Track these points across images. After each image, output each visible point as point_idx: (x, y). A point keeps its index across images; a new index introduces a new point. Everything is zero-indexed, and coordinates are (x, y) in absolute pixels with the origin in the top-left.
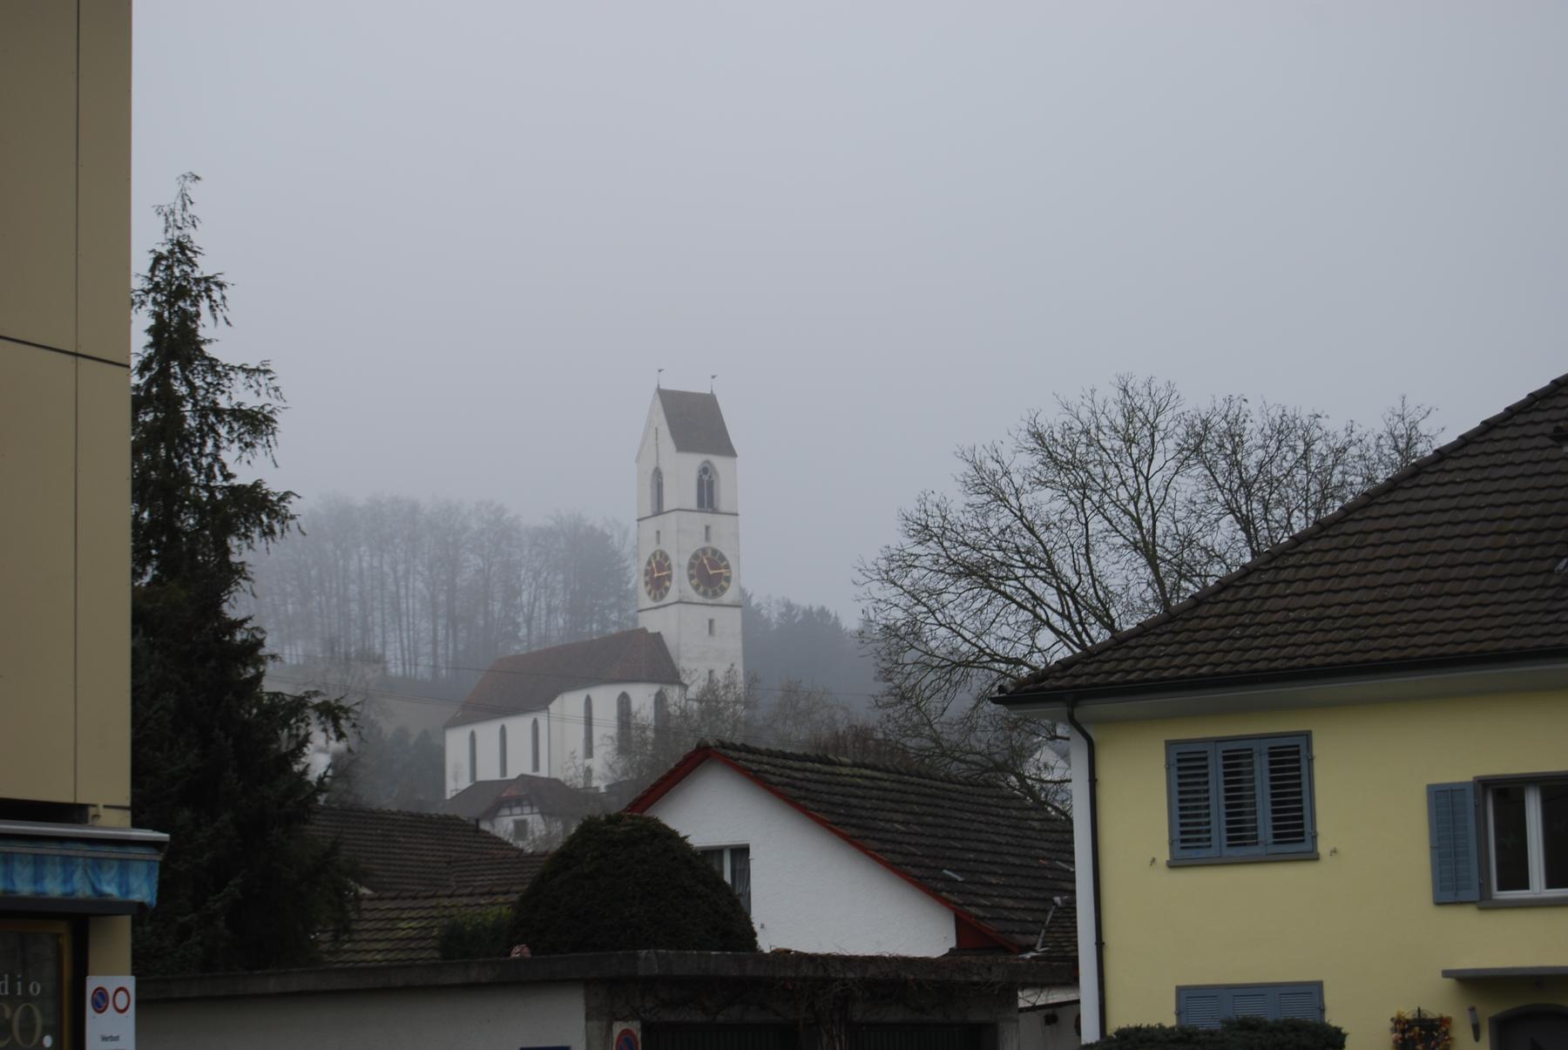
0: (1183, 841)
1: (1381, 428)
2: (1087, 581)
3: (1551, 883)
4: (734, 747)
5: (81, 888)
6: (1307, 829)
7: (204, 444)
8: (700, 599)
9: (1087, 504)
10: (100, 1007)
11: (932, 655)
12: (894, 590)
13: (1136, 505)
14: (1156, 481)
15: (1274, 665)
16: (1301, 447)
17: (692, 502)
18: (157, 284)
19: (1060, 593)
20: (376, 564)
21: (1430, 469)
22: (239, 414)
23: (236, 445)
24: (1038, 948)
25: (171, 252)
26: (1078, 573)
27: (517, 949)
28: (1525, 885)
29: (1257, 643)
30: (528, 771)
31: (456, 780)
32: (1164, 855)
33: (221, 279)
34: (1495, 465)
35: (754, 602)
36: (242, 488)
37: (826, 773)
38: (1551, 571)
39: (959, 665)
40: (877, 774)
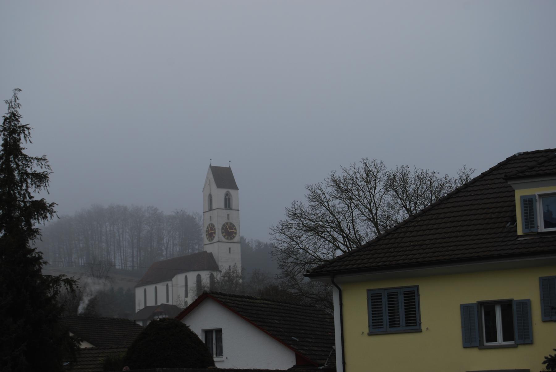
0: (373, 326)
1: (456, 177)
2: (352, 232)
3: (505, 340)
4: (217, 293)
6: (418, 321)
7: (22, 186)
8: (226, 240)
9: (353, 205)
11: (298, 259)
12: (284, 236)
13: (370, 205)
14: (377, 196)
15: (405, 262)
16: (429, 183)
17: (223, 206)
18: (5, 128)
19: (344, 237)
20: (112, 229)
21: (462, 191)
23: (34, 186)
24: (325, 365)
25: (10, 117)
26: (349, 230)
27: (125, 368)
28: (496, 340)
29: (399, 254)
30: (165, 302)
31: (139, 306)
32: (367, 331)
33: (28, 126)
34: (485, 189)
35: (247, 241)
36: (36, 201)
37: (250, 302)
38: (504, 227)
39: (308, 263)
40: (270, 302)
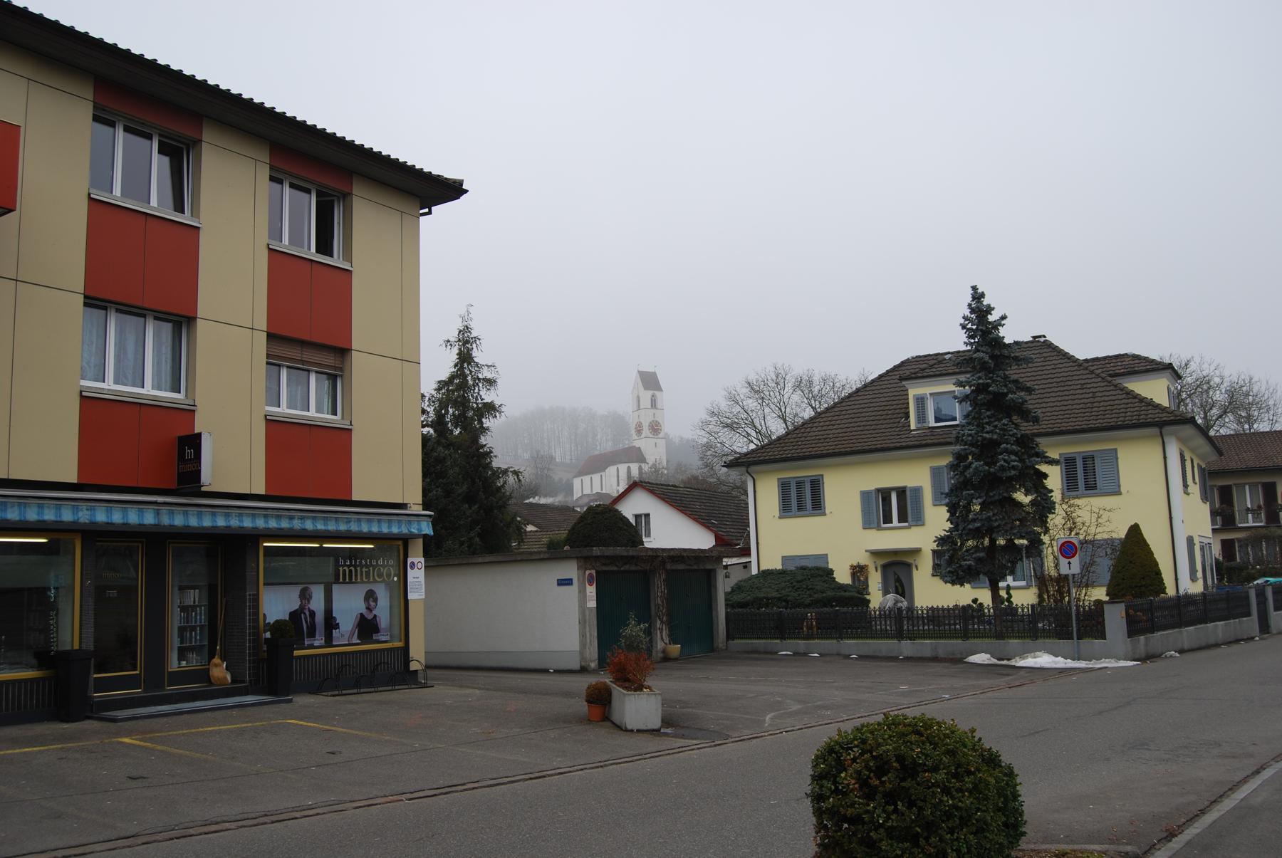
5: (404, 530)
10: (412, 568)
14: (786, 396)
22: (486, 380)
32: (777, 514)
